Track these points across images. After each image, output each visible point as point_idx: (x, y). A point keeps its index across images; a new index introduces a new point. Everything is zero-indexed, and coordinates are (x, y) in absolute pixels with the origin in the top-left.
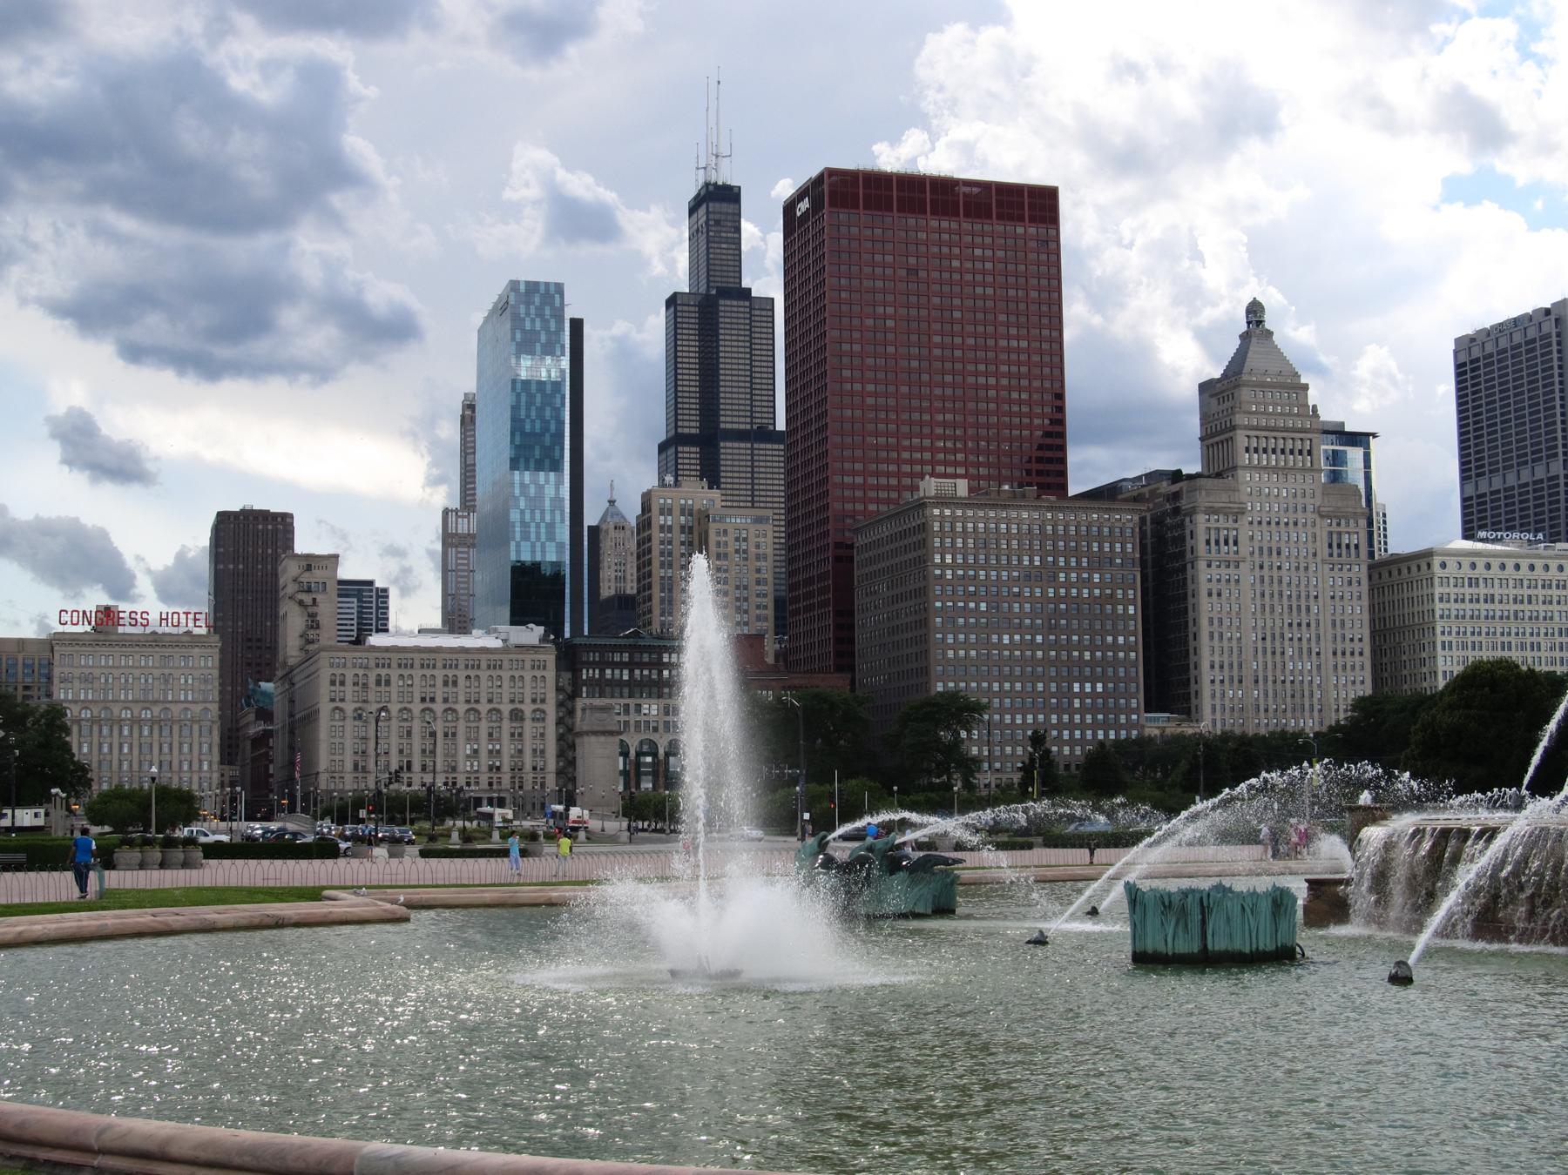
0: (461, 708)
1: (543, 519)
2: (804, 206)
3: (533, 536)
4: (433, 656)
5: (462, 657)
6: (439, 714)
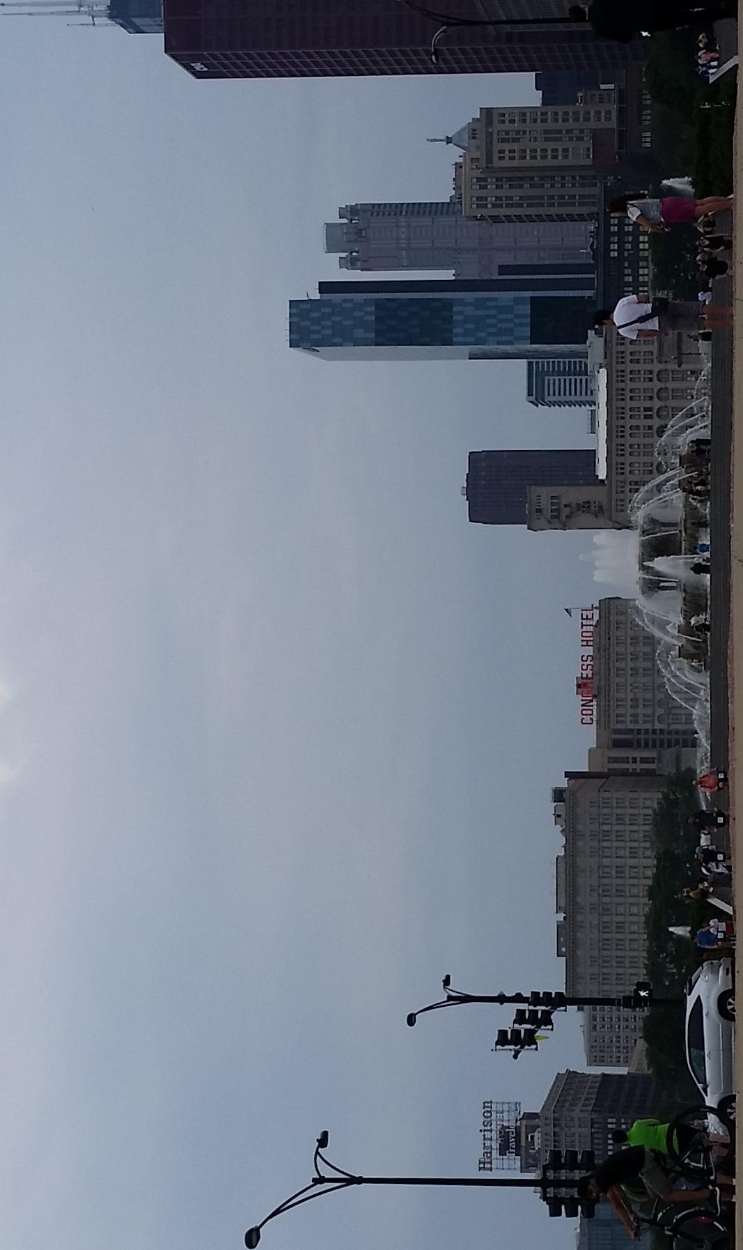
0: (656, 385)
1: (494, 317)
2: (198, 67)
3: (509, 325)
4: (614, 429)
5: (615, 441)
6: (662, 366)
